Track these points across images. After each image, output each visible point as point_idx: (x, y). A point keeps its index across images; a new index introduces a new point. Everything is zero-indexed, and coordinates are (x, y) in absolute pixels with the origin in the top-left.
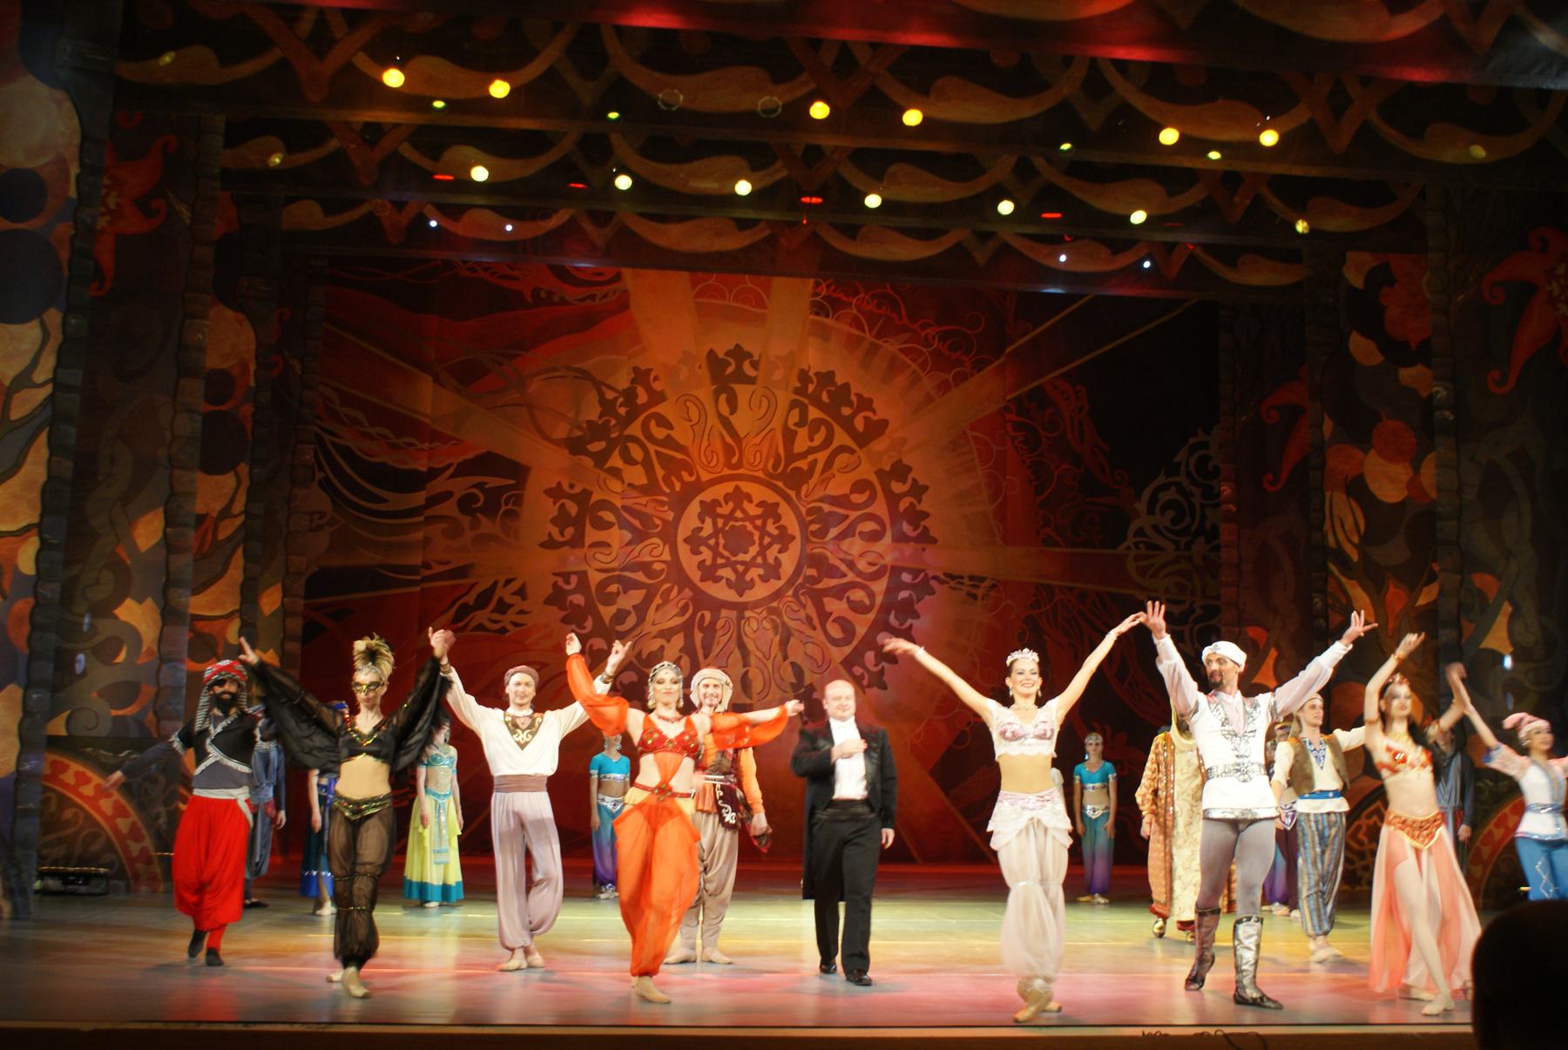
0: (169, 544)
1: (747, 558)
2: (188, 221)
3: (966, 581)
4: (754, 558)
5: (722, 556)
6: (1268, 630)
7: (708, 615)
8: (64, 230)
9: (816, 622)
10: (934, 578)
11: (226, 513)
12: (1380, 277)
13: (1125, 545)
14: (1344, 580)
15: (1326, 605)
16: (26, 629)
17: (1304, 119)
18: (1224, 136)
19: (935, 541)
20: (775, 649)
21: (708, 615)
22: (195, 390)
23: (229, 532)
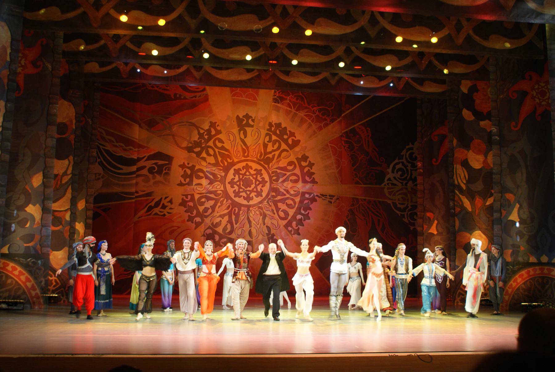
0: (45, 185)
1: (250, 189)
2: (51, 70)
3: (328, 197)
4: (253, 189)
5: (242, 188)
6: (434, 214)
7: (237, 209)
9: (275, 212)
10: (317, 196)
11: (65, 174)
12: (473, 89)
13: (384, 184)
14: (460, 196)
15: (454, 205)
17: (447, 33)
19: (317, 183)
20: (261, 221)
21: (237, 209)
22: (53, 130)
23: (66, 180)
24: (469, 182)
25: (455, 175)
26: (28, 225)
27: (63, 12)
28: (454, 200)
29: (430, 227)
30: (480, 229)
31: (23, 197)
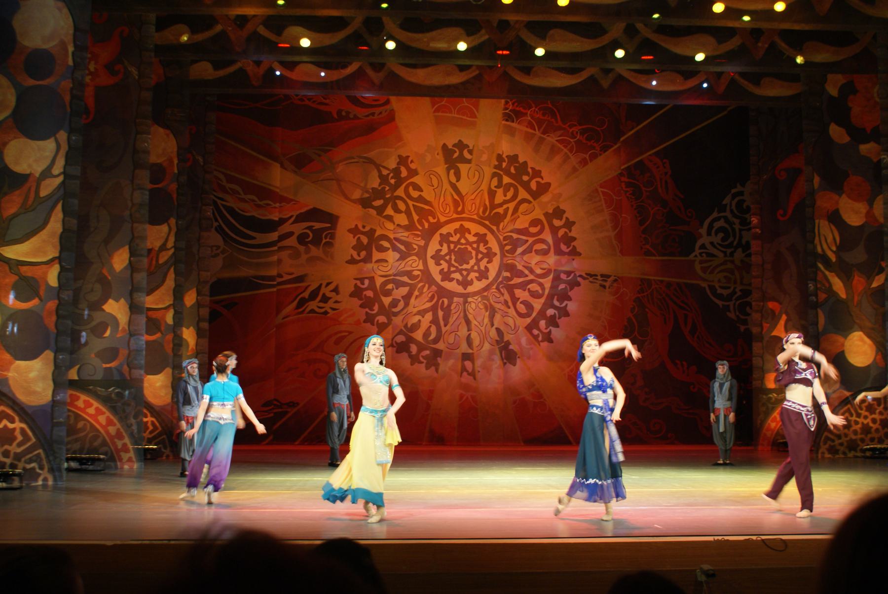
0: (132, 267)
6: (781, 304)
8: (67, 84)
11: (163, 248)
12: (848, 90)
14: (827, 273)
15: (817, 288)
16: (54, 318)
18: (752, 7)
22: (144, 177)
24: (842, 248)
25: (817, 238)
28: (815, 280)
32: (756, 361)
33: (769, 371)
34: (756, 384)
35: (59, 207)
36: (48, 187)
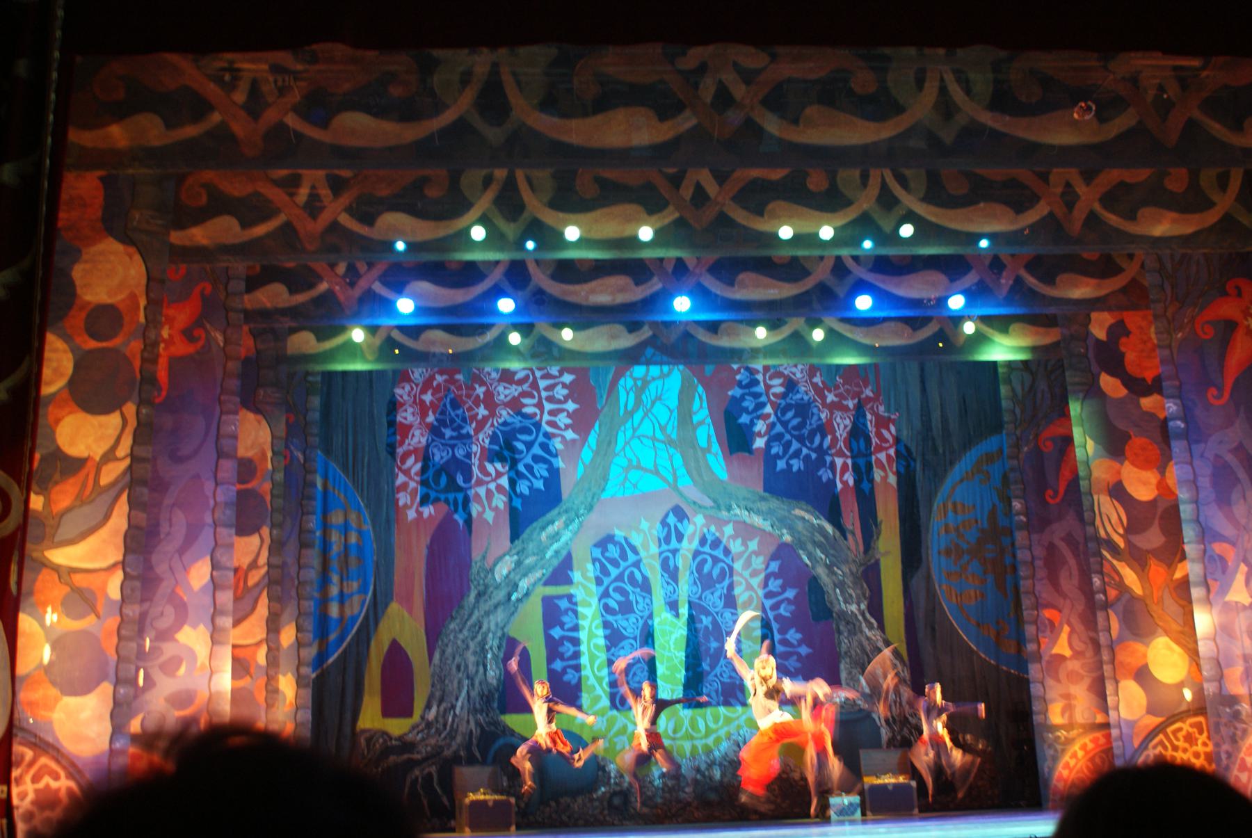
0: (215, 585)
6: (1060, 611)
8: (136, 346)
11: (254, 565)
12: (1118, 331)
14: (1115, 562)
15: (1104, 583)
16: (115, 640)
17: (1045, 212)
18: (988, 229)
22: (228, 468)
24: (1132, 528)
25: (1098, 518)
26: (182, 670)
27: (245, 225)
28: (1101, 573)
29: (1054, 641)
30: (1167, 633)
31: (170, 611)
32: (1035, 689)
33: (1053, 701)
34: (1037, 719)
35: (125, 497)
36: (110, 474)
